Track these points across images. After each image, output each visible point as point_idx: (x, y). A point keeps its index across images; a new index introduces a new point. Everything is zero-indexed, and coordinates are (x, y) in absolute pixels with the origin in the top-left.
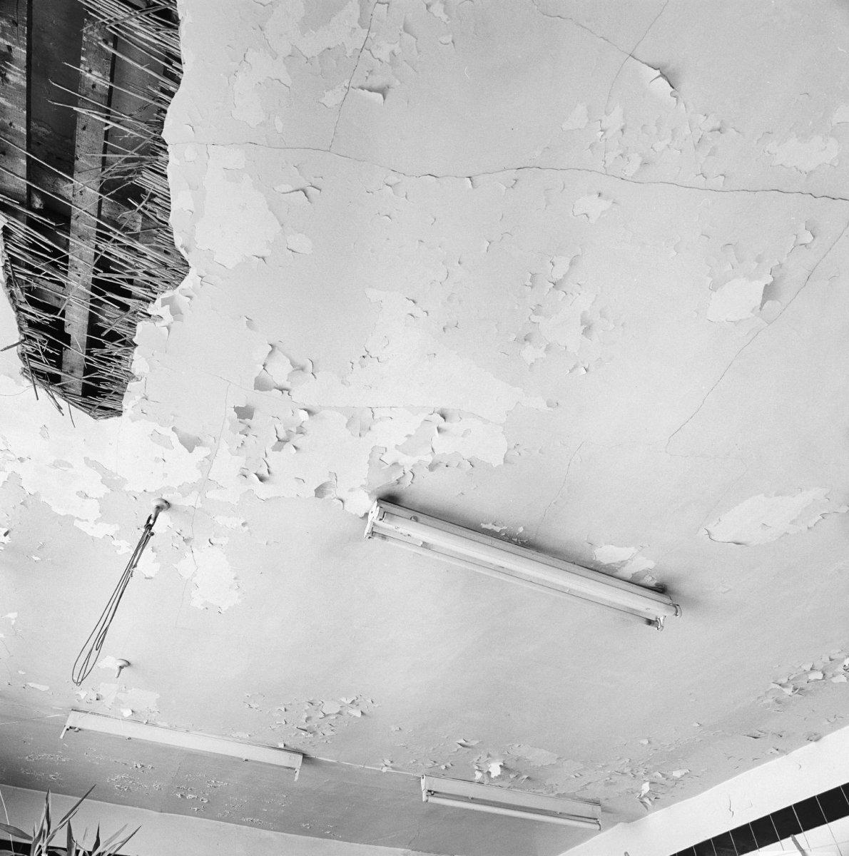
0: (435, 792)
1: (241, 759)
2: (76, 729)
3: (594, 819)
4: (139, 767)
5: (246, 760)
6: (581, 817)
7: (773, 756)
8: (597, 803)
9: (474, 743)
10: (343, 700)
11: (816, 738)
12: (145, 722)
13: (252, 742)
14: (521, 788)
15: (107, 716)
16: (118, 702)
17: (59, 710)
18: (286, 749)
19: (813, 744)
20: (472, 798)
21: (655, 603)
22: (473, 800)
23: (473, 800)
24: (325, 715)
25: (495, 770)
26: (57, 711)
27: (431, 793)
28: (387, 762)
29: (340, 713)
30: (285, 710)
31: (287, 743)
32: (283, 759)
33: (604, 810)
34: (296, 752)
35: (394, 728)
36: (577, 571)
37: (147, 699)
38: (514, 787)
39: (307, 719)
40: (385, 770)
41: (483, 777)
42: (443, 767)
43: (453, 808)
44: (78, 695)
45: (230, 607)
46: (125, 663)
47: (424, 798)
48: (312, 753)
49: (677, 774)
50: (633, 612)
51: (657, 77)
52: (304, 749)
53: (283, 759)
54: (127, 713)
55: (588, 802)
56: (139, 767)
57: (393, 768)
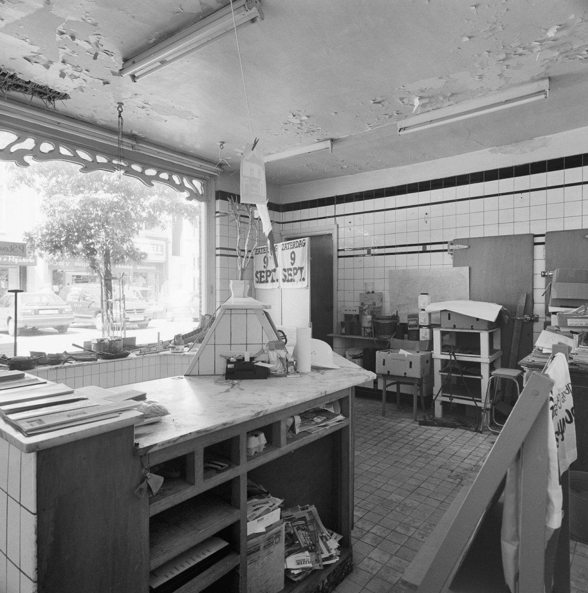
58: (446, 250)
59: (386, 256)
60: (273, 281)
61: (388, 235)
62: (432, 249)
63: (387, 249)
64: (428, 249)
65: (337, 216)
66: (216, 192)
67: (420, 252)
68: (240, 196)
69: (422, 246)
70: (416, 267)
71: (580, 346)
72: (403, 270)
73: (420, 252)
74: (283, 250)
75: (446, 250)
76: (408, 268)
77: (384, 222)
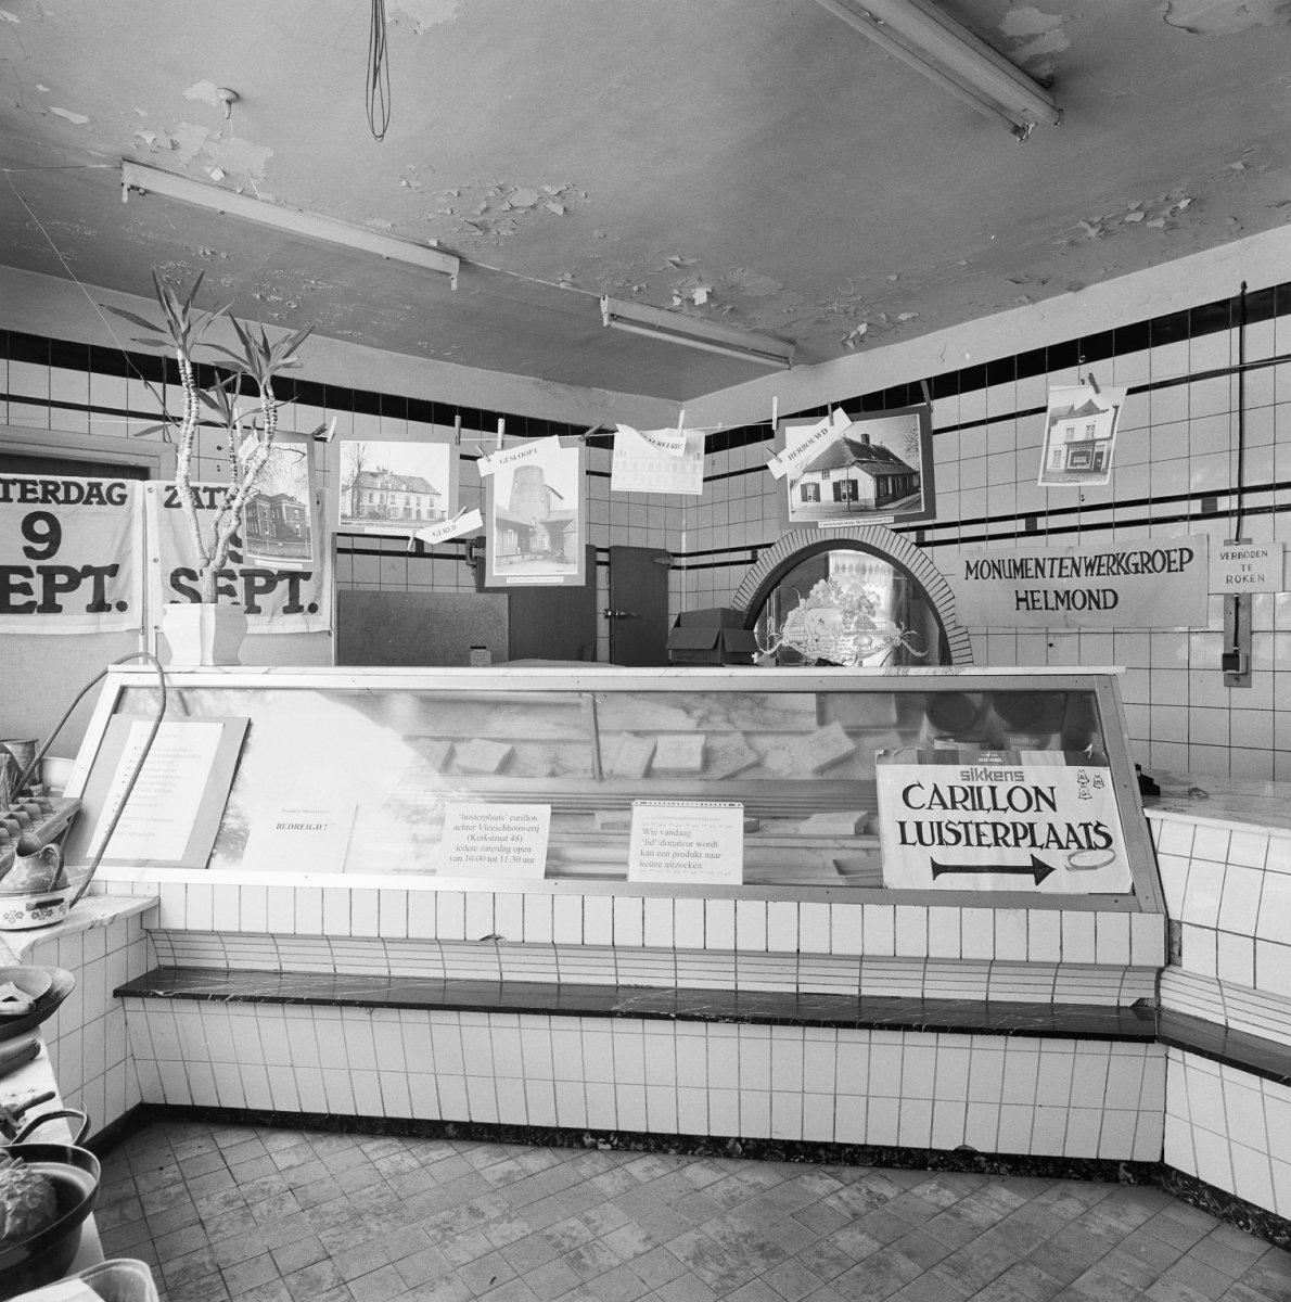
0: (618, 317)
1: (381, 256)
2: (142, 191)
3: (785, 359)
4: (208, 253)
5: (388, 258)
6: (7, 441)
7: (1021, 303)
8: (791, 342)
9: (690, 262)
10: (547, 188)
11: (1076, 287)
12: (239, 191)
13: (392, 234)
14: (714, 320)
15: (181, 176)
16: (202, 156)
17: (102, 158)
18: (441, 249)
19: (1071, 293)
20: (660, 327)
21: (1038, 101)
22: (661, 329)
23: (661, 329)
24: (512, 208)
25: (700, 296)
26: (99, 160)
27: (613, 316)
28: (568, 276)
29: (534, 207)
30: (459, 194)
31: (443, 241)
32: (435, 261)
33: (799, 351)
34: (451, 253)
35: (596, 233)
36: (1010, 71)
37: (252, 158)
38: (708, 319)
39: (487, 210)
40: (562, 286)
41: (681, 305)
42: (635, 288)
43: (629, 333)
44: (138, 137)
45: (445, 22)
46: (233, 96)
47: (606, 323)
48: (472, 255)
49: (903, 317)
50: (999, 108)
51: (831, 947)
52: (463, 251)
53: (435, 261)
54: (217, 175)
55: (783, 339)
56: (208, 253)
57: (573, 285)
58: (462, 557)
59: (1082, 514)
60: (99, 606)
61: (1272, 717)
62: (1118, 519)
63: (1142, 517)
64: (1023, 522)
65: (967, 1105)
66: (706, 437)
67: (1042, 514)
68: (1143, 793)
69: (914, 533)
70: (403, 589)
71: (1103, 466)
72: (373, 592)
73: (1042, 514)
74: (113, 570)
75: (462, 557)
76: (412, 589)
77: (962, 463)
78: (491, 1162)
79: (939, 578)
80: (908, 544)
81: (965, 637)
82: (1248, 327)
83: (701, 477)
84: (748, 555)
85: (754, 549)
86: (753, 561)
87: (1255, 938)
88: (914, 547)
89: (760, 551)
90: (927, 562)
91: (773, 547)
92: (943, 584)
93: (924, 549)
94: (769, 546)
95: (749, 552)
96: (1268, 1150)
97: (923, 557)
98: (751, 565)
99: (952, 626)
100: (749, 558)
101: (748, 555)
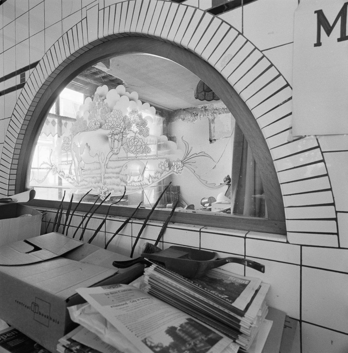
78: (229, 276)
79: (257, 55)
80: (199, 13)
81: (316, 155)
82: (287, 230)
83: (104, 250)
84: (16, 81)
85: (22, 72)
86: (21, 86)
87: (10, 174)
88: (209, 16)
89: (27, 73)
90: (233, 33)
91: (38, 66)
92: (265, 64)
93: (224, 16)
94: (34, 65)
95: (18, 77)
96: (5, 51)
97: (225, 27)
98: (19, 91)
99: (286, 137)
100: (19, 83)
101: (16, 81)
